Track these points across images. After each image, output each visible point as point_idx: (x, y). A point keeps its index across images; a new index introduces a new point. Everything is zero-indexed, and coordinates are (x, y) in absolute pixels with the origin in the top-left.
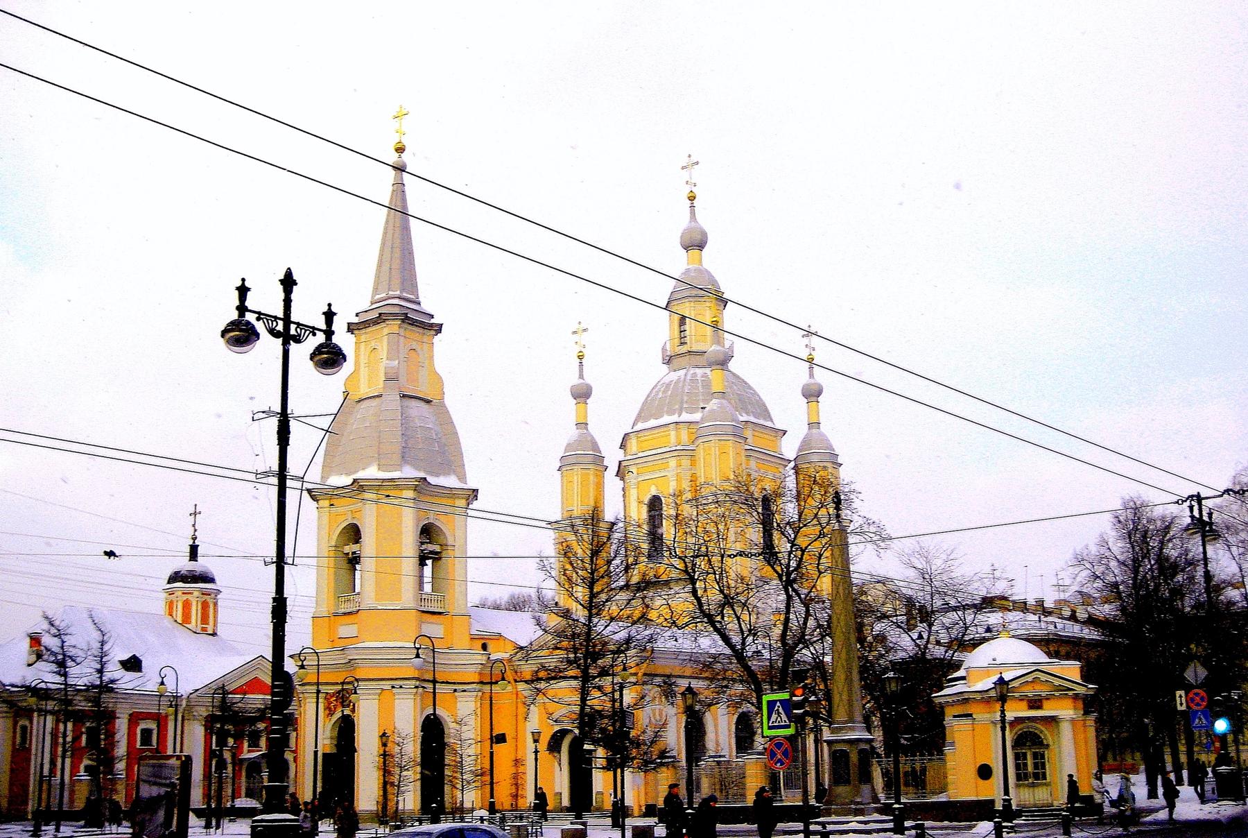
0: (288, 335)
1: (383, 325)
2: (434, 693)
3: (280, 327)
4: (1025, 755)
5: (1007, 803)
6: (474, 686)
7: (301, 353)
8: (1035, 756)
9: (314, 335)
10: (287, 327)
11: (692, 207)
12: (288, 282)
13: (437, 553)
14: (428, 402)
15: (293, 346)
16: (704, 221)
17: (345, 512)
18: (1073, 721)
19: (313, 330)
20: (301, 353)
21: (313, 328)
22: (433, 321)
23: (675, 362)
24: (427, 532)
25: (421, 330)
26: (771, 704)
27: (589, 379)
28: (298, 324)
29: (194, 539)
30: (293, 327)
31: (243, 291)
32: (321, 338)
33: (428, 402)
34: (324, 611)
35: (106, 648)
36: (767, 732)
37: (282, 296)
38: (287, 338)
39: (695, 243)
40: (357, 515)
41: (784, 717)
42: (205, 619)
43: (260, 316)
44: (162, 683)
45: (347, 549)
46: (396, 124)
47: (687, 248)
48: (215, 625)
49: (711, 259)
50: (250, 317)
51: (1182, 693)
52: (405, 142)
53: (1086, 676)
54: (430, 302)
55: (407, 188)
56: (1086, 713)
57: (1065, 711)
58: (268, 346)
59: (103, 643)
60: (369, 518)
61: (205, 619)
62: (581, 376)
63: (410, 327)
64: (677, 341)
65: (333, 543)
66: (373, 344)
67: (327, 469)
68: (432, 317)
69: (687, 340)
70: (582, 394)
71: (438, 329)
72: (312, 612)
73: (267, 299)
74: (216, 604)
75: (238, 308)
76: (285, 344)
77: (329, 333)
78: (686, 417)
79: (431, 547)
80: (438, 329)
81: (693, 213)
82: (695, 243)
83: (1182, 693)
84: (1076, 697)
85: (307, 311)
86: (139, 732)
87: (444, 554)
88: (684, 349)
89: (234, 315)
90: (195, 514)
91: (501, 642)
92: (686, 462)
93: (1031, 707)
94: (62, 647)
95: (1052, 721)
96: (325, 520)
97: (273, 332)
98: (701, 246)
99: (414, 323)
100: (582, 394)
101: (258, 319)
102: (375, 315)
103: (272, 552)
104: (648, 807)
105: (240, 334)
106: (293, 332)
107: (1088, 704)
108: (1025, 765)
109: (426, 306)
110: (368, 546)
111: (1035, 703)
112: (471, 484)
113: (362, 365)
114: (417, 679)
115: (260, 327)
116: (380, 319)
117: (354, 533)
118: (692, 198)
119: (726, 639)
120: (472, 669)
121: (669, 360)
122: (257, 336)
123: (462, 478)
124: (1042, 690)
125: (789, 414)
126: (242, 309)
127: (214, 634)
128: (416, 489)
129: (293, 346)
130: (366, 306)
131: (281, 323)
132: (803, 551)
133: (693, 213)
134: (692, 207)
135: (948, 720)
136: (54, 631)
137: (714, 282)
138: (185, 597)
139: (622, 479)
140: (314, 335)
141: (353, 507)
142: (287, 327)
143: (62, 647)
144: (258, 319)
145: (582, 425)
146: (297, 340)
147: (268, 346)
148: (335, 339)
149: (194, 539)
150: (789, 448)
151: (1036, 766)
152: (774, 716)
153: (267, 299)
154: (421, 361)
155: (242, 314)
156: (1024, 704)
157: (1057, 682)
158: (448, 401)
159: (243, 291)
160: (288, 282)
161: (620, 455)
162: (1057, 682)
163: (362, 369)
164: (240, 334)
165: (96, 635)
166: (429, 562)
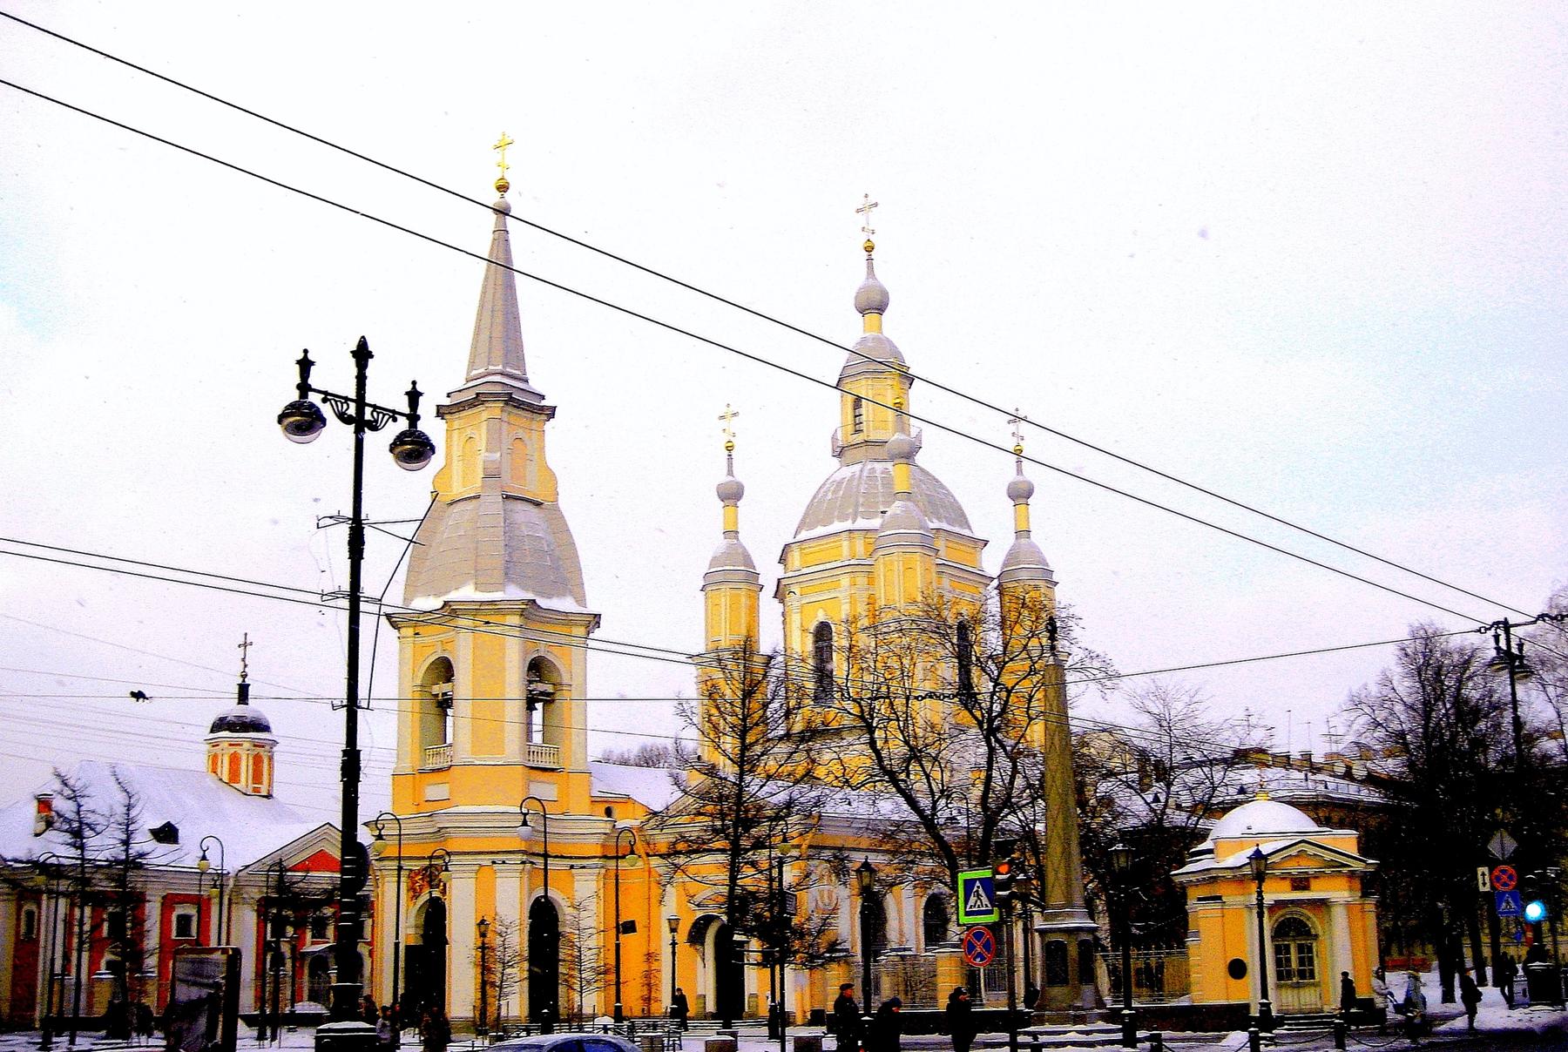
0: (361, 421)
1: (481, 408)
2: (546, 870)
3: (352, 411)
4: (1287, 948)
5: (1266, 1008)
6: (595, 861)
7: (378, 443)
8: (1300, 949)
9: (395, 420)
10: (360, 411)
11: (870, 259)
12: (362, 354)
13: (549, 694)
14: (538, 504)
15: (368, 435)
16: (885, 277)
17: (434, 643)
18: (1348, 905)
19: (394, 415)
20: (378, 443)
21: (394, 412)
22: (543, 403)
23: (848, 454)
24: (537, 667)
25: (529, 415)
26: (969, 884)
27: (740, 476)
28: (375, 407)
29: (244, 676)
30: (368, 410)
31: (305, 365)
32: (403, 424)
33: (538, 504)
34: (407, 767)
35: (133, 813)
36: (964, 919)
37: (355, 371)
38: (361, 425)
39: (874, 305)
40: (448, 647)
41: (985, 900)
42: (257, 777)
43: (327, 397)
44: (204, 858)
45: (436, 689)
46: (497, 155)
47: (863, 311)
48: (270, 785)
49: (893, 325)
50: (314, 398)
51: (1486, 870)
52: (509, 178)
53: (1365, 849)
54: (540, 379)
55: (511, 237)
56: (1365, 895)
57: (1339, 892)
58: (337, 434)
59: (129, 807)
60: (464, 650)
61: (257, 777)
62: (730, 473)
63: (515, 411)
64: (850, 429)
65: (419, 682)
66: (468, 432)
67: (411, 589)
68: (543, 397)
69: (864, 427)
70: (731, 495)
71: (551, 412)
72: (391, 768)
73: (335, 375)
74: (271, 759)
75: (299, 387)
76: (359, 432)
77: (413, 418)
78: (861, 523)
79: (541, 687)
80: (551, 412)
81: (870, 268)
82: (874, 305)
83: (1486, 870)
84: (1352, 875)
85: (385, 390)
86: (174, 919)
87: (557, 696)
88: (860, 438)
89: (295, 396)
90: (245, 645)
91: (630, 806)
92: (861, 580)
93: (1295, 888)
94: (78, 813)
95: (1322, 905)
96: (409, 653)
97: (343, 417)
98: (880, 309)
99: (520, 405)
100: (731, 495)
101: (324, 401)
102: (471, 395)
103: (342, 693)
104: (814, 1013)
105: (302, 419)
106: (368, 417)
107: (1367, 883)
108: (1288, 960)
109: (535, 385)
110: (462, 685)
111: (1301, 883)
112: (592, 608)
113: (455, 458)
114: (524, 852)
115: (327, 410)
116: (478, 401)
117: (445, 669)
118: (869, 249)
119: (912, 802)
120: (593, 839)
121: (840, 452)
122: (324, 421)
123: (581, 600)
124: (1310, 867)
125: (991, 520)
126: (304, 388)
127: (269, 796)
128: (522, 613)
129: (368, 435)
130: (460, 384)
131: (353, 406)
132: (1009, 692)
133: (870, 268)
134: (870, 259)
135: (1191, 904)
136: (67, 792)
137: (897, 354)
138: (233, 749)
139: (782, 601)
140: (395, 420)
141: (443, 637)
142: (360, 411)
143: (78, 813)
144: (324, 401)
145: (731, 533)
146: (374, 426)
147: (337, 434)
148: (421, 426)
149: (244, 676)
150: (991, 563)
151: (1301, 962)
152: (973, 899)
153: (335, 375)
154: (529, 453)
155: (304, 395)
156: (1287, 884)
157: (1328, 856)
158: (563, 504)
159: (305, 365)
160: (362, 354)
161: (779, 571)
162: (1328, 856)
163: (455, 463)
164: (302, 419)
165: (121, 798)
166: (539, 706)
